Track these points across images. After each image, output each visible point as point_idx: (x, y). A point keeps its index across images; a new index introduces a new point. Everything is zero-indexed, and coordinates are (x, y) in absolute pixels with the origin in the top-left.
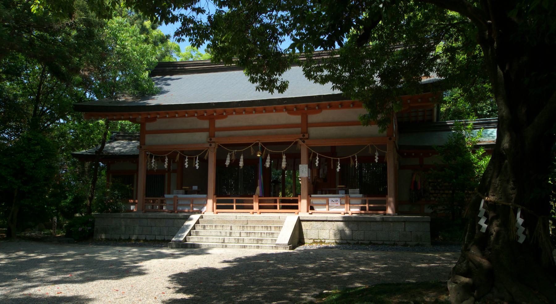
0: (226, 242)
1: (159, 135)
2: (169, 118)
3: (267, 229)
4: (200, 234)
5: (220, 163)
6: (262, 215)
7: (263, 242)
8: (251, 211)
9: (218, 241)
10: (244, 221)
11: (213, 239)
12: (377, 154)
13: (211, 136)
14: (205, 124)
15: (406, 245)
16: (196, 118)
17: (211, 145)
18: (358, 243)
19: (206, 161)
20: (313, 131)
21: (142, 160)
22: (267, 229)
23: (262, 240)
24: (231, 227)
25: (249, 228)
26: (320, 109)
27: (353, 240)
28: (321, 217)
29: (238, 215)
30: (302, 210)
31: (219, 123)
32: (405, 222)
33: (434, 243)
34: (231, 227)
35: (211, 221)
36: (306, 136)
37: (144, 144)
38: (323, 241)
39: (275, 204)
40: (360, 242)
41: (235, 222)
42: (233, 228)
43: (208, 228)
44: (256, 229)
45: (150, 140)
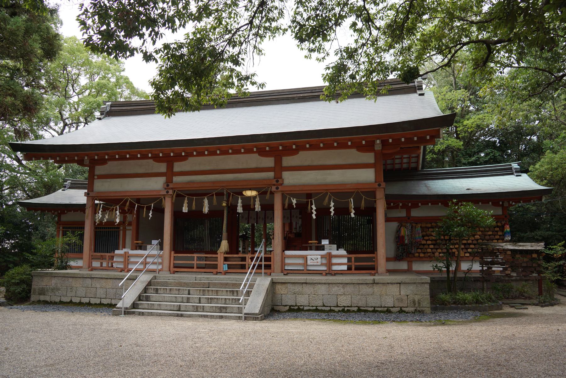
0: (182, 309)
1: (109, 180)
2: (119, 159)
3: (233, 294)
4: (151, 299)
5: (177, 214)
6: (176, 275)
7: (228, 311)
8: (214, 271)
9: (172, 308)
10: (205, 283)
11: (167, 305)
12: (332, 204)
13: (169, 182)
14: (162, 167)
15: (401, 311)
16: (257, 155)
17: (167, 192)
18: (343, 311)
19: (162, 211)
20: (176, 179)
21: (88, 211)
22: (233, 294)
23: (226, 308)
24: (189, 290)
25: (210, 293)
26: (301, 148)
27: (337, 306)
28: (299, 279)
29: (199, 276)
30: (275, 270)
31: (178, 167)
32: (400, 283)
33: (434, 309)
34: (189, 290)
35: (165, 284)
36: (280, 182)
37: (93, 191)
38: (301, 307)
39: (198, 262)
40: (346, 309)
41: (194, 285)
42: (191, 292)
43: (162, 292)
44: (220, 293)
45: (101, 186)
